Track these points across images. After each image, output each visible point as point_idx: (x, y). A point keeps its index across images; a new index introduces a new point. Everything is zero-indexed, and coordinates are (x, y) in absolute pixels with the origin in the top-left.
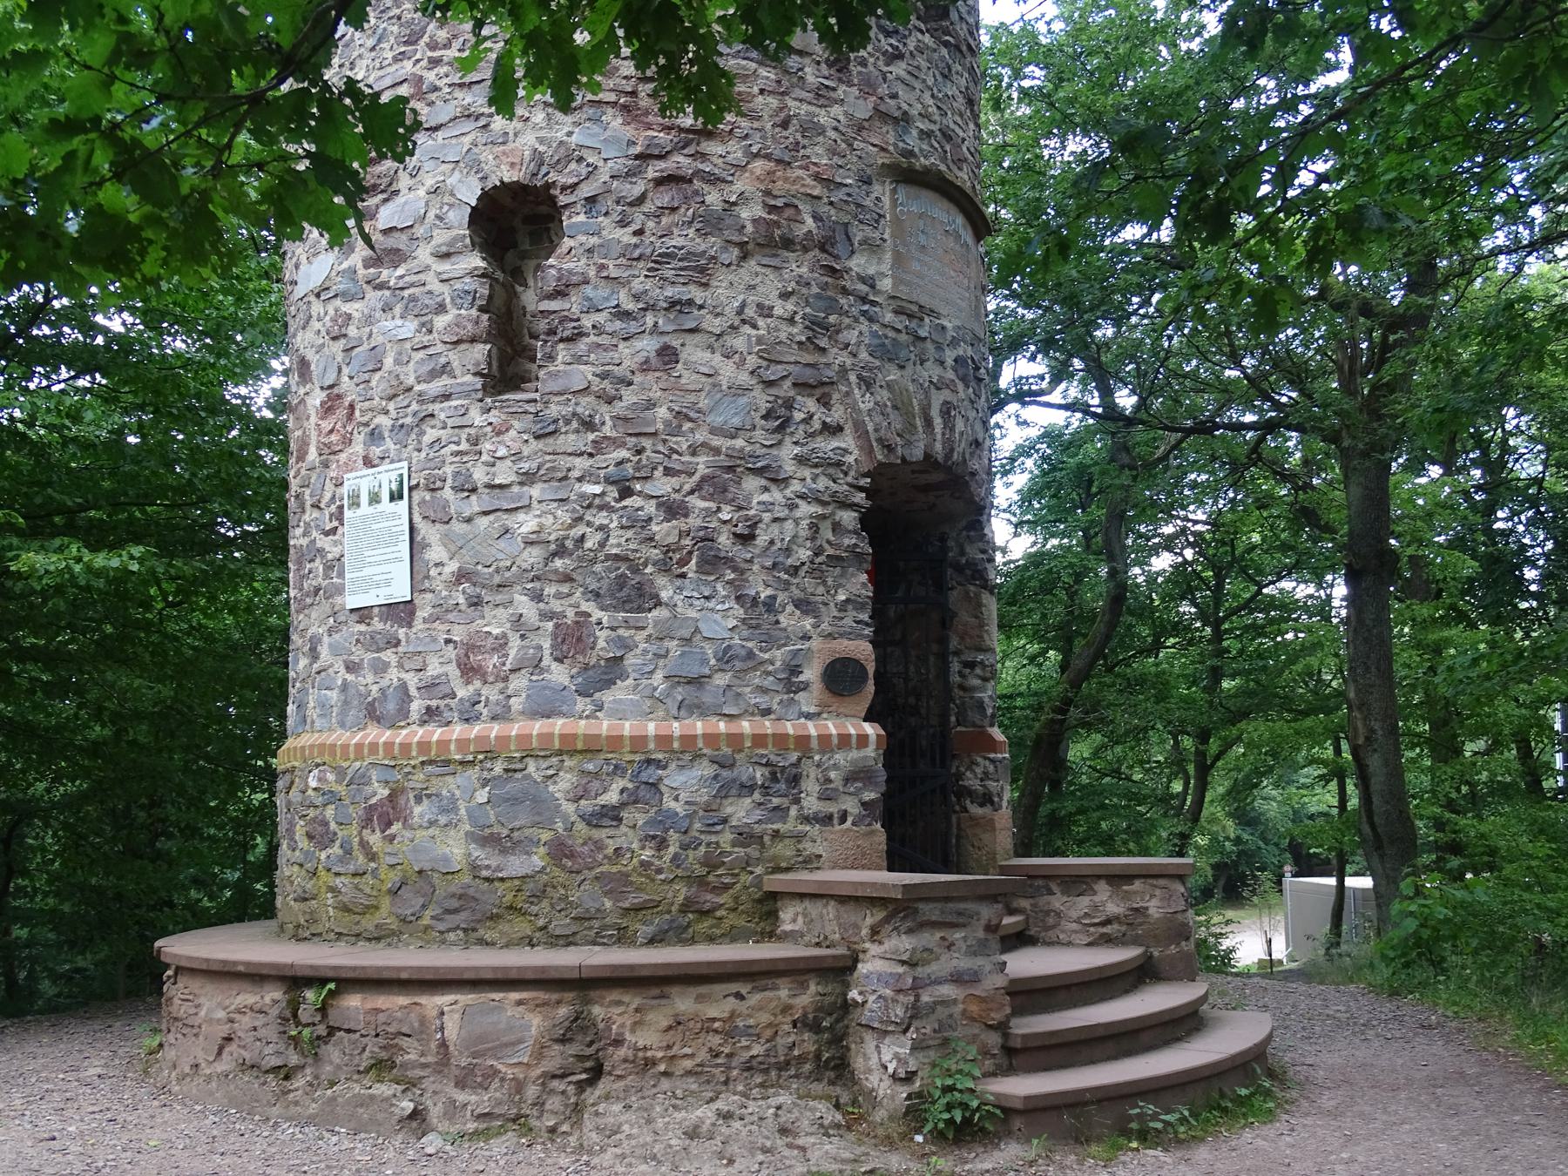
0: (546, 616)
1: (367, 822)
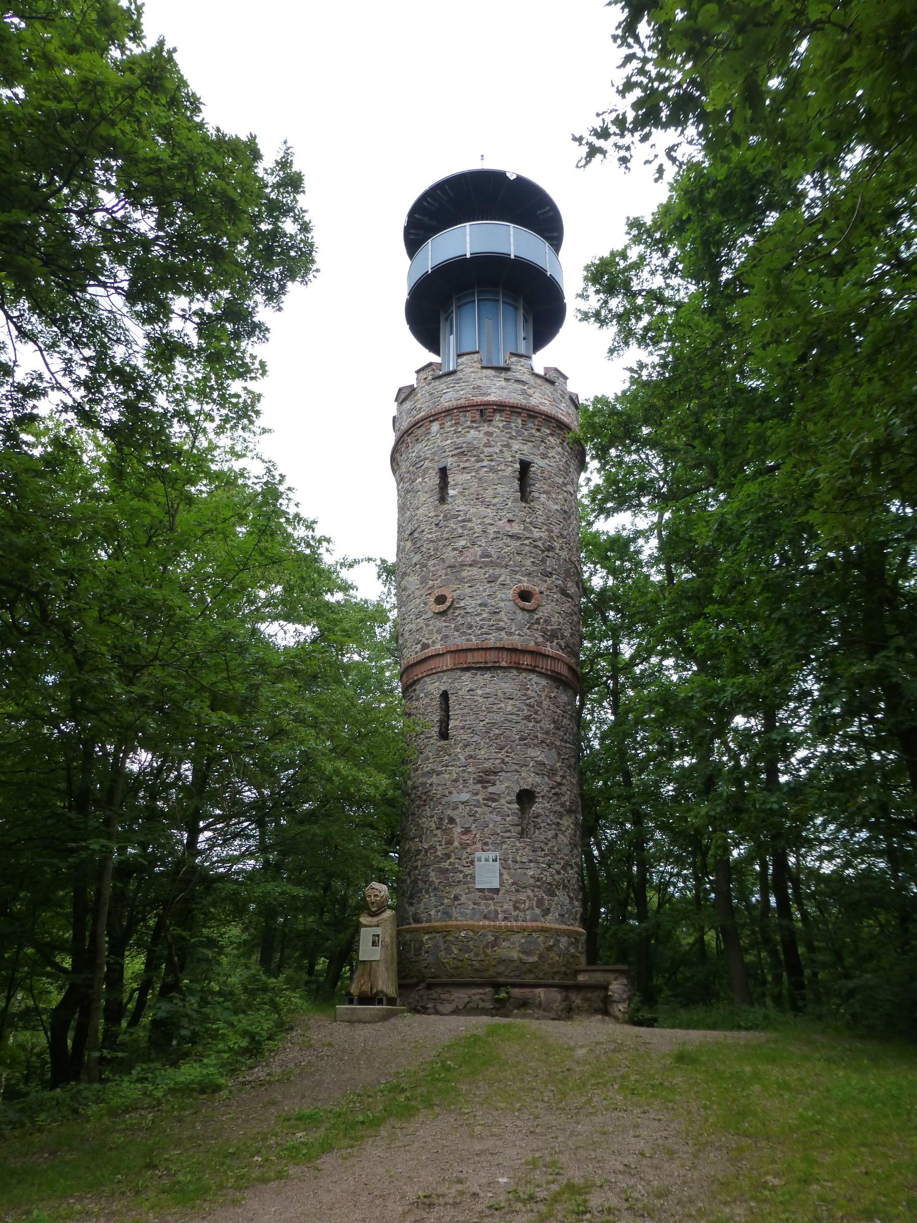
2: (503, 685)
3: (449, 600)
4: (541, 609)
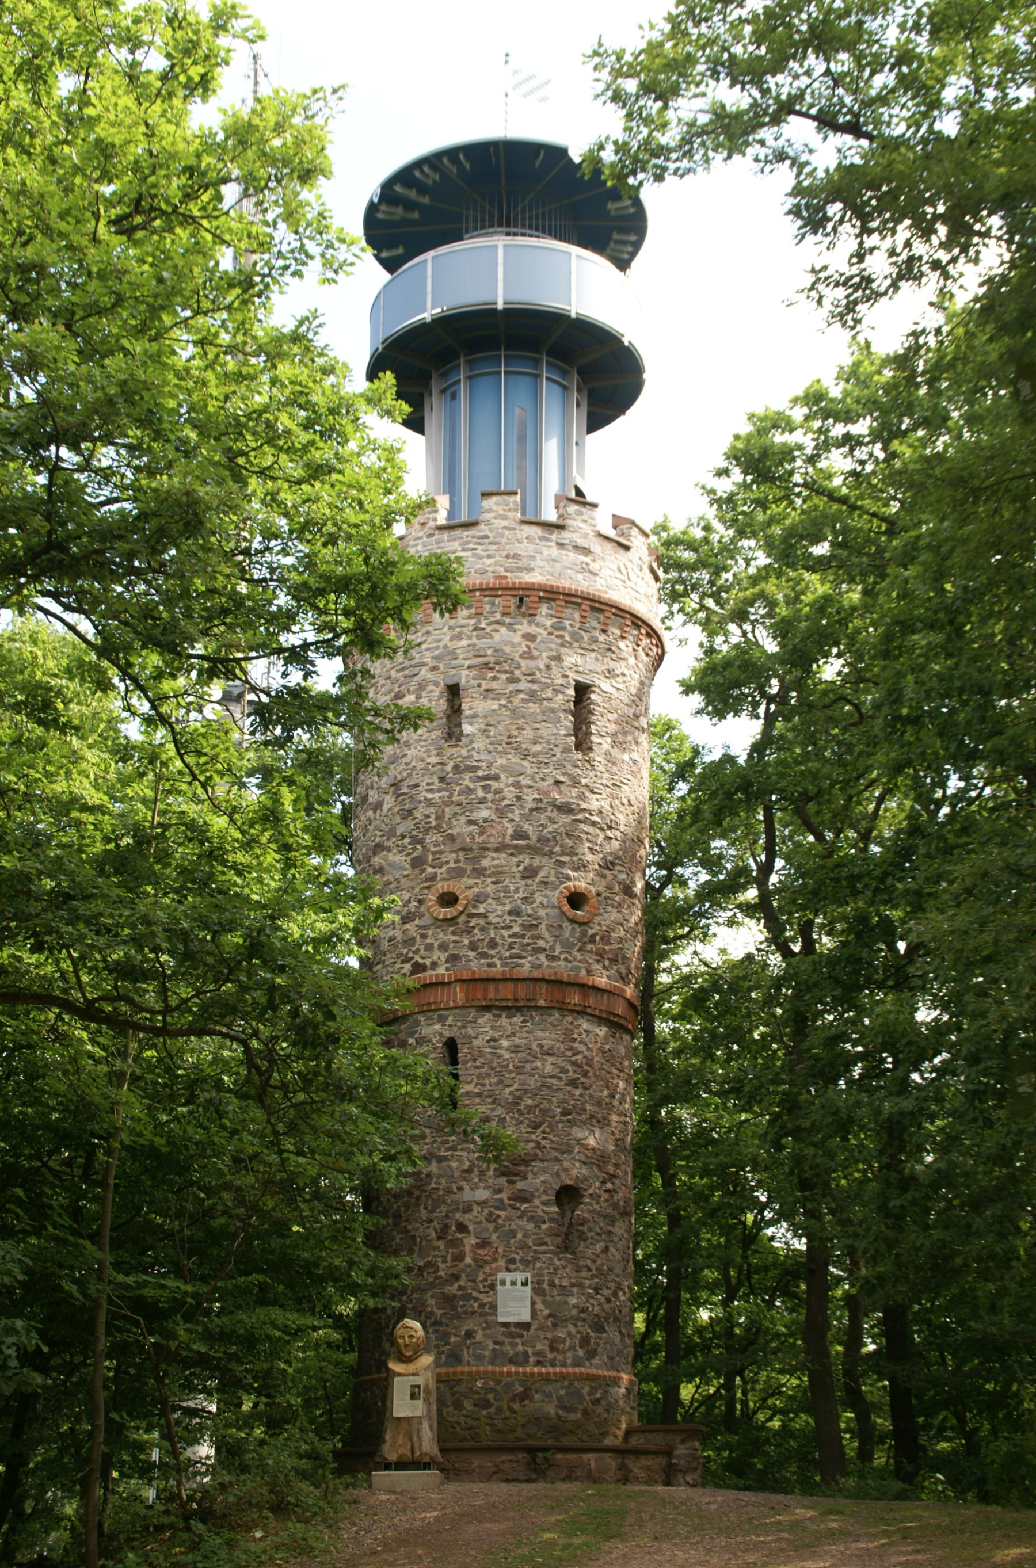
0: (578, 1332)
1: (513, 1399)
2: (540, 1034)
3: (462, 902)
4: (597, 919)
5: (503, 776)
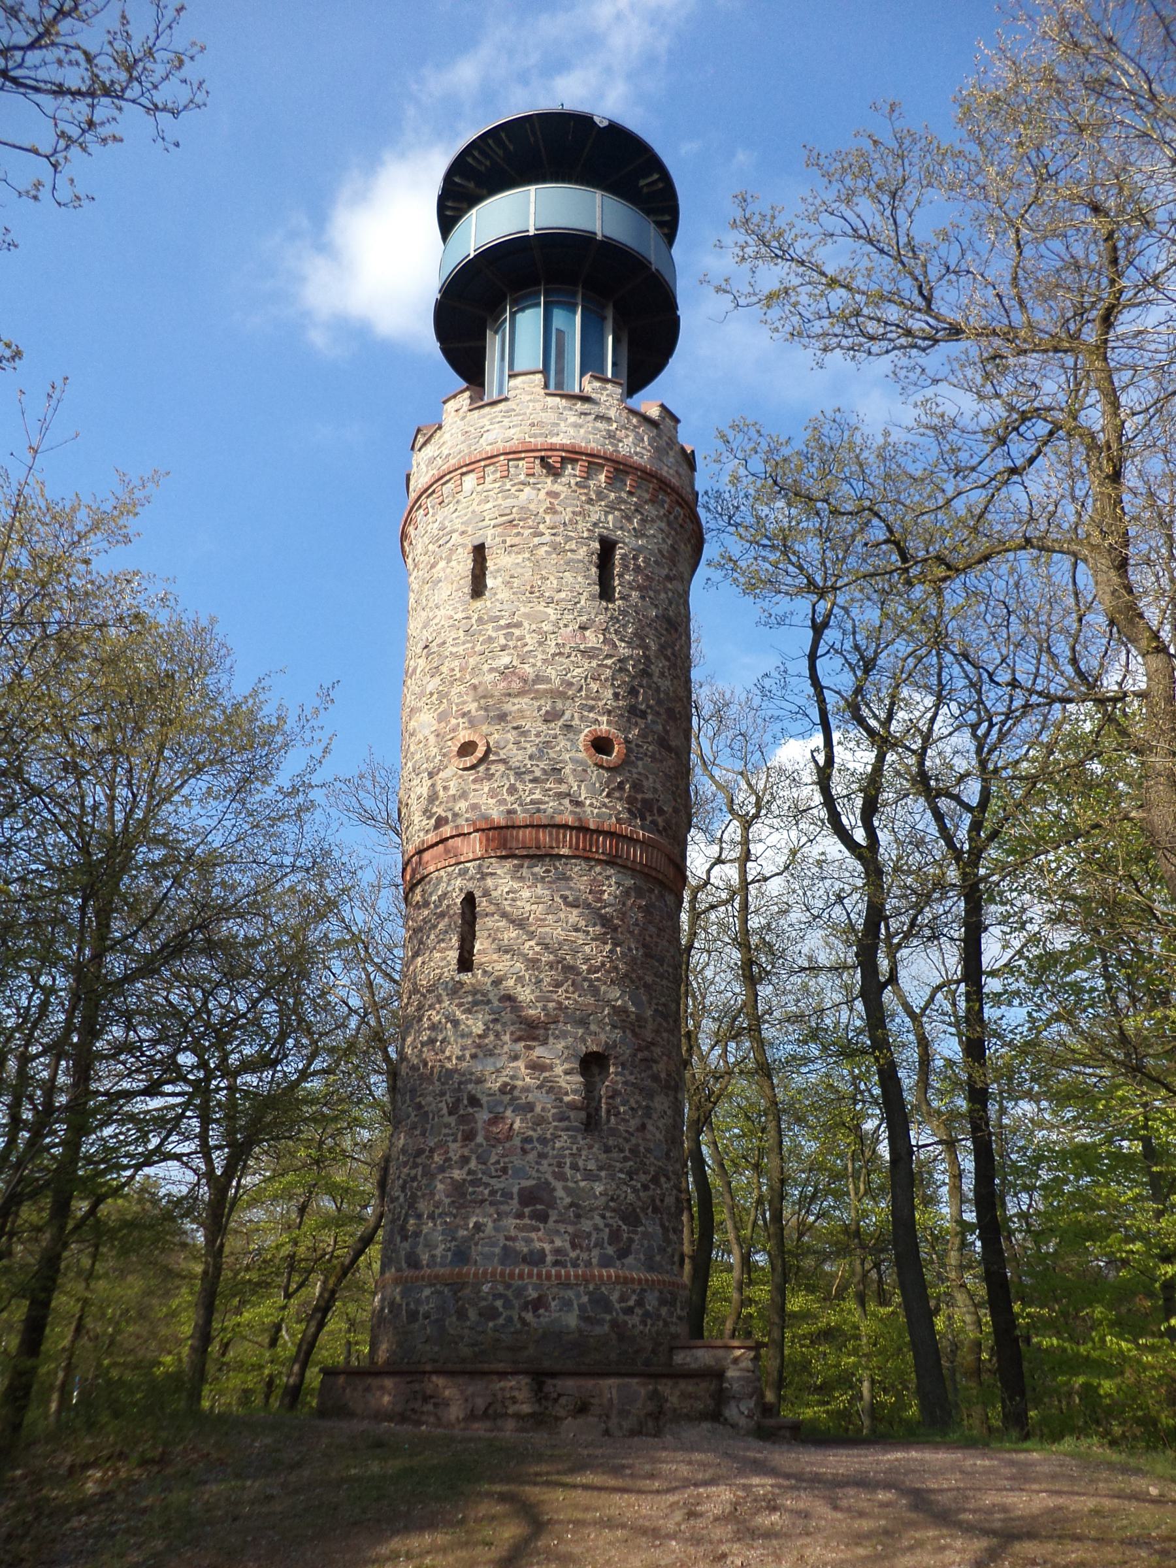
0: (607, 1225)
1: (525, 1307)
5: (526, 624)
